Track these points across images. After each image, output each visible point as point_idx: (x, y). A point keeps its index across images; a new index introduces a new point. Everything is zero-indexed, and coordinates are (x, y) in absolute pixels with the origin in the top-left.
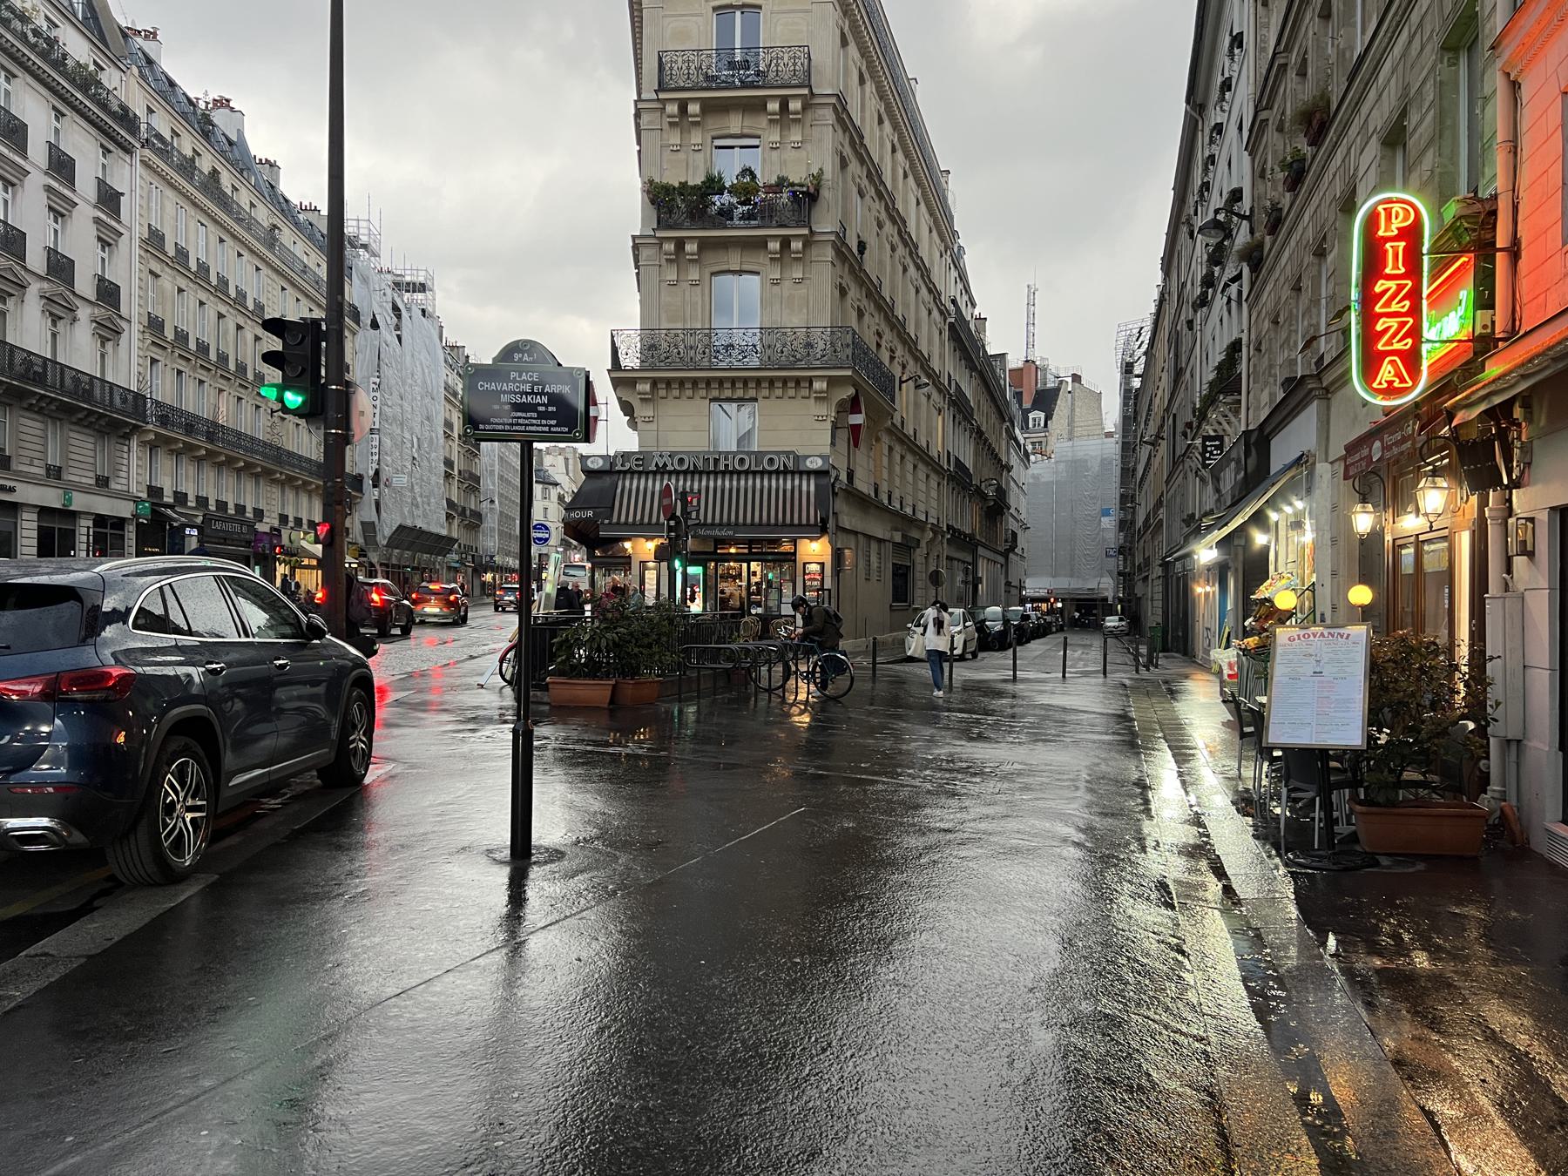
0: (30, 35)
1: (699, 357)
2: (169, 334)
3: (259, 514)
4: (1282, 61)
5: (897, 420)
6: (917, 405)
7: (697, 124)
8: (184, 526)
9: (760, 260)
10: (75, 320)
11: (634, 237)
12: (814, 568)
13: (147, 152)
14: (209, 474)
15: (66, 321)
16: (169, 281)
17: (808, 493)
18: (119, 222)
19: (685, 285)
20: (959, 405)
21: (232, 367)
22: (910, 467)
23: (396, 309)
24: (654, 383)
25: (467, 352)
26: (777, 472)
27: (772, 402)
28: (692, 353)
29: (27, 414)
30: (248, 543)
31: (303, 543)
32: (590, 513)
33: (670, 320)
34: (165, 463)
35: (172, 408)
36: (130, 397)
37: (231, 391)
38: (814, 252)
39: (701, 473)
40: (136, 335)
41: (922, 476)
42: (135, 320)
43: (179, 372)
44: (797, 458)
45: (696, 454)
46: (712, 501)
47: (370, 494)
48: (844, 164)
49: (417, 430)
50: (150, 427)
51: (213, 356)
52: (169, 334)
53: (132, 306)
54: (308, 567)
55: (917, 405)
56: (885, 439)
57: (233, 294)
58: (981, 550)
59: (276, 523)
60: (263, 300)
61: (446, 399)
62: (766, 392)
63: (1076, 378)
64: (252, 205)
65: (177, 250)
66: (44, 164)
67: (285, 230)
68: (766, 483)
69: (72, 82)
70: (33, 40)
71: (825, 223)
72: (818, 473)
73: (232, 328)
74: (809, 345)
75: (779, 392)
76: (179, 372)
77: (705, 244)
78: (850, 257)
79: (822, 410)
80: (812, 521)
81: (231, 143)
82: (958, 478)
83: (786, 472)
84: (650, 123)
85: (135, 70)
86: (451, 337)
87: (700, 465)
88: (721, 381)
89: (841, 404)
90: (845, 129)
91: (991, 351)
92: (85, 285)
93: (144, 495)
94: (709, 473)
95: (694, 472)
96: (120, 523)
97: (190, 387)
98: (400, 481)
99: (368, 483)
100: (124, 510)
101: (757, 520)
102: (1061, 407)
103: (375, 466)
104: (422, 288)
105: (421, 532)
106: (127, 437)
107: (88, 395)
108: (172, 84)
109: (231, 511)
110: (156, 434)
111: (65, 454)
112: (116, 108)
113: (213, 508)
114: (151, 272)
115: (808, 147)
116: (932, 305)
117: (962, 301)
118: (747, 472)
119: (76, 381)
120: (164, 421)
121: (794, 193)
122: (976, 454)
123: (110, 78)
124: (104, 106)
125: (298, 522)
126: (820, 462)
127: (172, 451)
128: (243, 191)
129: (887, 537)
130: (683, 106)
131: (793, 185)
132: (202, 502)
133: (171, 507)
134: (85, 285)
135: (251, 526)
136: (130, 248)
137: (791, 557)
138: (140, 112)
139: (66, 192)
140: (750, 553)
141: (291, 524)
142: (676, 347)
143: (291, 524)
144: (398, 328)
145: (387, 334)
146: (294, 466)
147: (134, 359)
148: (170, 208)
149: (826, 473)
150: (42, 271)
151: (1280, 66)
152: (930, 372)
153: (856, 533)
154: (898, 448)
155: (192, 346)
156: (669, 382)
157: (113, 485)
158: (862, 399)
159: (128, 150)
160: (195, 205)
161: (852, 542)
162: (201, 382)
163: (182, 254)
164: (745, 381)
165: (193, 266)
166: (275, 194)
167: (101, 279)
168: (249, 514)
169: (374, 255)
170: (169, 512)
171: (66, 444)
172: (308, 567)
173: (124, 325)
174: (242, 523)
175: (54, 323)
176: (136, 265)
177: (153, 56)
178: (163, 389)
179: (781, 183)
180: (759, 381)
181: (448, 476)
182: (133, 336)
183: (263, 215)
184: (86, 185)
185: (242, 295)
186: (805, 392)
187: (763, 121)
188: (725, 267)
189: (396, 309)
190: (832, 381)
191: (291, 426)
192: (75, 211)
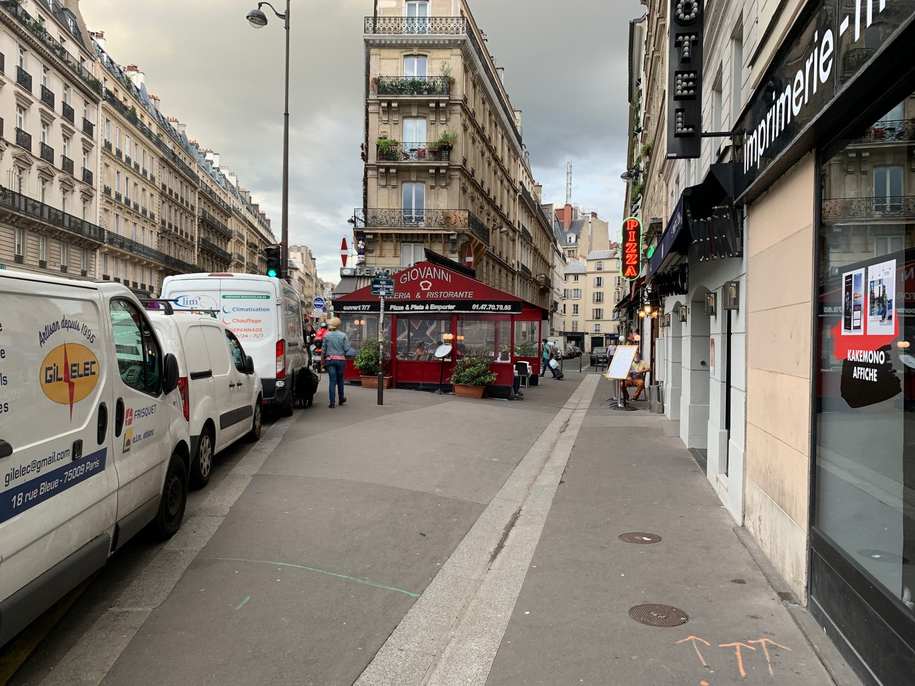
6: (501, 239)
13: (105, 102)
15: (70, 192)
16: (114, 168)
18: (53, 111)
22: (497, 271)
29: (4, 225)
40: (99, 197)
41: (503, 275)
42: (99, 189)
48: (465, 129)
53: (98, 183)
55: (501, 239)
63: (594, 215)
64: (150, 124)
66: (61, 113)
67: (165, 136)
76: (117, 215)
92: (78, 174)
102: (586, 231)
106: (95, 250)
109: (139, 288)
119: (76, 223)
122: (534, 261)
123: (88, 65)
134: (78, 174)
139: (70, 126)
146: (140, 252)
147: (99, 210)
150: (81, 179)
157: (89, 275)
159: (96, 102)
162: (127, 220)
167: (85, 170)
176: (99, 161)
182: (98, 198)
184: (79, 123)
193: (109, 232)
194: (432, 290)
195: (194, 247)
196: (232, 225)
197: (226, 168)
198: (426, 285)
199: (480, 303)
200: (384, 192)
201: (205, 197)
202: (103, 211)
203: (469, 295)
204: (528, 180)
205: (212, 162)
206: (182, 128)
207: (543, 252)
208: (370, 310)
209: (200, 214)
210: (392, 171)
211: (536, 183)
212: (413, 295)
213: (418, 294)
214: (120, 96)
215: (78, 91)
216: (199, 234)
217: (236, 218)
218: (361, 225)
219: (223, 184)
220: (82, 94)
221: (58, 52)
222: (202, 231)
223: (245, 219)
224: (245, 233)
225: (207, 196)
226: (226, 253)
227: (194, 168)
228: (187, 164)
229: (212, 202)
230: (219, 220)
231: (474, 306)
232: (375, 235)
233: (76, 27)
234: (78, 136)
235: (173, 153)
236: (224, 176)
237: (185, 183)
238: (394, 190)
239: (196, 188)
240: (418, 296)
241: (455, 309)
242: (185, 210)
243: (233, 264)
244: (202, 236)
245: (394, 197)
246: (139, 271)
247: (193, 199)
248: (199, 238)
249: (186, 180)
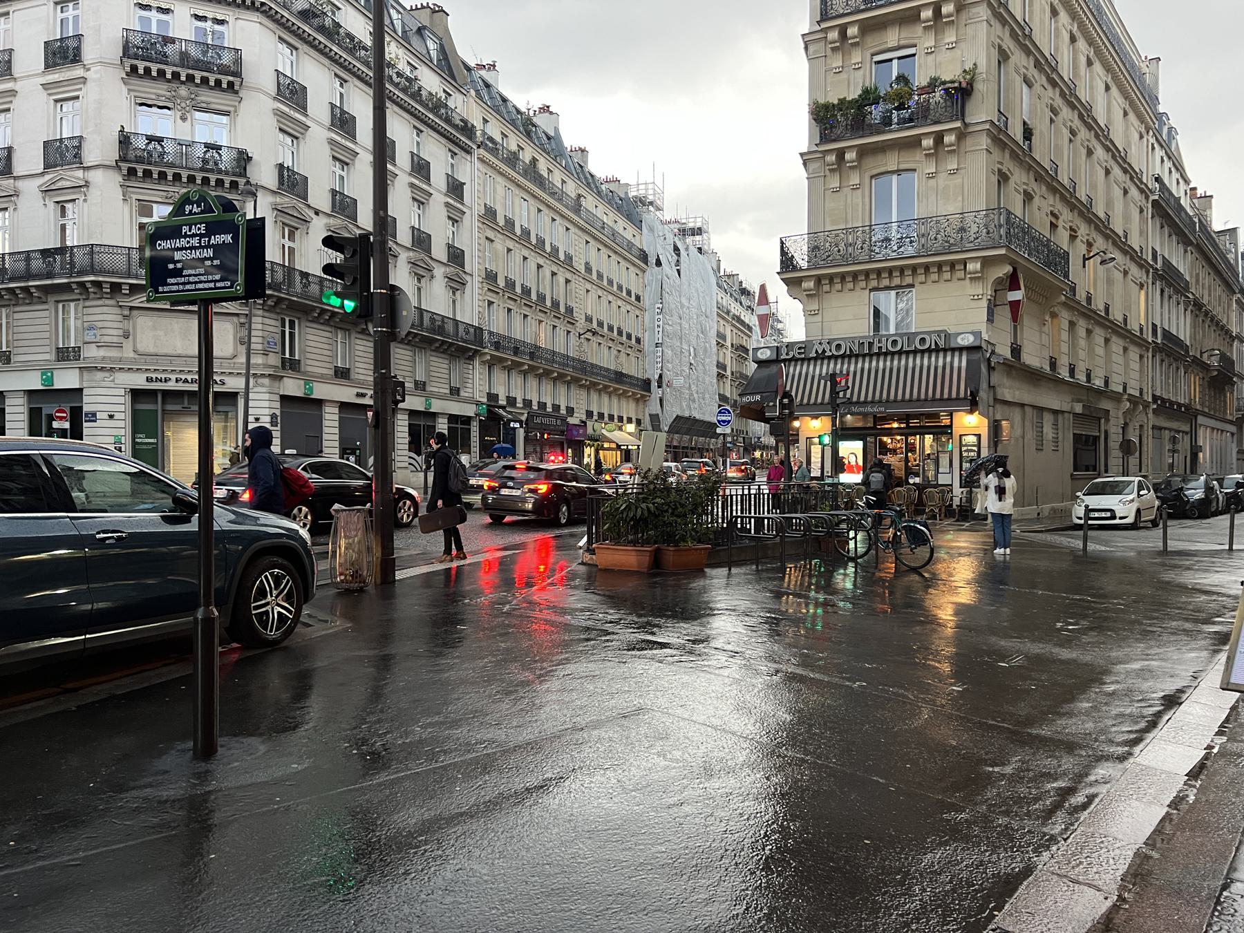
0: (395, 76)
2: (501, 282)
3: (570, 411)
5: (1081, 296)
7: (856, 44)
8: (510, 421)
9: (914, 159)
10: (432, 277)
11: (802, 155)
12: (972, 439)
13: (481, 151)
14: (532, 383)
16: (501, 244)
17: (960, 368)
19: (846, 190)
20: (1168, 279)
21: (548, 303)
22: (1082, 332)
23: (676, 249)
24: (819, 280)
25: (741, 278)
26: (929, 350)
27: (929, 287)
28: (850, 249)
30: (562, 433)
31: (604, 432)
32: (758, 397)
33: (833, 223)
34: (500, 376)
35: (505, 337)
36: (472, 330)
37: (548, 321)
38: (969, 142)
39: (857, 356)
40: (477, 285)
42: (476, 274)
43: (509, 310)
44: (948, 336)
45: (852, 340)
46: (863, 379)
47: (656, 392)
48: (1003, 56)
49: (694, 342)
51: (534, 297)
52: (501, 282)
53: (473, 264)
54: (609, 449)
55: (1110, 281)
56: (1065, 316)
57: (548, 249)
58: (1201, 419)
59: (584, 417)
60: (572, 252)
61: (719, 315)
62: (922, 278)
65: (506, 221)
66: (408, 167)
67: (590, 198)
68: (881, 364)
69: (426, 106)
70: (396, 80)
71: (981, 112)
72: (970, 349)
73: (548, 274)
74: (962, 230)
75: (935, 277)
76: (509, 310)
77: (863, 152)
78: (1013, 146)
79: (978, 289)
80: (962, 395)
81: (549, 138)
82: (1169, 349)
83: (937, 350)
84: (815, 52)
85: (473, 92)
86: (726, 267)
87: (856, 349)
88: (878, 272)
89: (999, 281)
90: (1004, 22)
91: (1217, 225)
92: (439, 252)
93: (485, 400)
94: (864, 356)
95: (850, 356)
96: (467, 420)
97: (517, 321)
98: (679, 382)
99: (654, 384)
100: (470, 410)
101: (907, 396)
103: (659, 371)
104: (698, 231)
105: (695, 420)
107: (441, 330)
108: (505, 100)
109: (549, 409)
111: (428, 372)
112: (458, 122)
113: (535, 407)
115: (962, 45)
116: (1129, 184)
117: (1171, 181)
118: (900, 353)
120: (497, 346)
121: (946, 90)
122: (1194, 326)
124: (448, 120)
125: (601, 416)
126: (971, 338)
128: (556, 172)
129: (1066, 407)
130: (843, 30)
131: (944, 83)
132: (528, 404)
133: (503, 408)
134: (439, 252)
135: (564, 420)
136: (471, 221)
137: (947, 431)
138: (478, 124)
139: (425, 186)
140: (908, 427)
141: (595, 417)
143: (595, 417)
144: (678, 263)
145: (668, 269)
148: (500, 191)
149: (979, 348)
150: (408, 244)
152: (1127, 251)
153: (1022, 405)
154: (1082, 324)
155: (518, 290)
156: (831, 278)
157: (462, 393)
158: (1021, 276)
159: (468, 151)
160: (519, 186)
161: (1016, 414)
163: (510, 223)
164: (902, 270)
165: (518, 231)
166: (583, 171)
168: (563, 411)
169: (658, 209)
170: (501, 411)
171: (428, 365)
172: (609, 449)
173: (468, 278)
174: (557, 418)
175: (419, 281)
177: (491, 81)
178: (497, 323)
179: (933, 84)
180: (914, 269)
181: (720, 376)
183: (571, 189)
185: (555, 250)
186: (961, 274)
187: (919, 29)
188: (883, 169)
189: (676, 249)
190: (987, 262)
191: (595, 345)
192: (431, 200)
193: (491, 333)
204: (1175, 175)
207: (1217, 311)
210: (848, 156)
211: (1200, 192)
220: (443, 141)
224: (728, 331)
233: (442, 49)
234: (439, 200)
246: (605, 398)
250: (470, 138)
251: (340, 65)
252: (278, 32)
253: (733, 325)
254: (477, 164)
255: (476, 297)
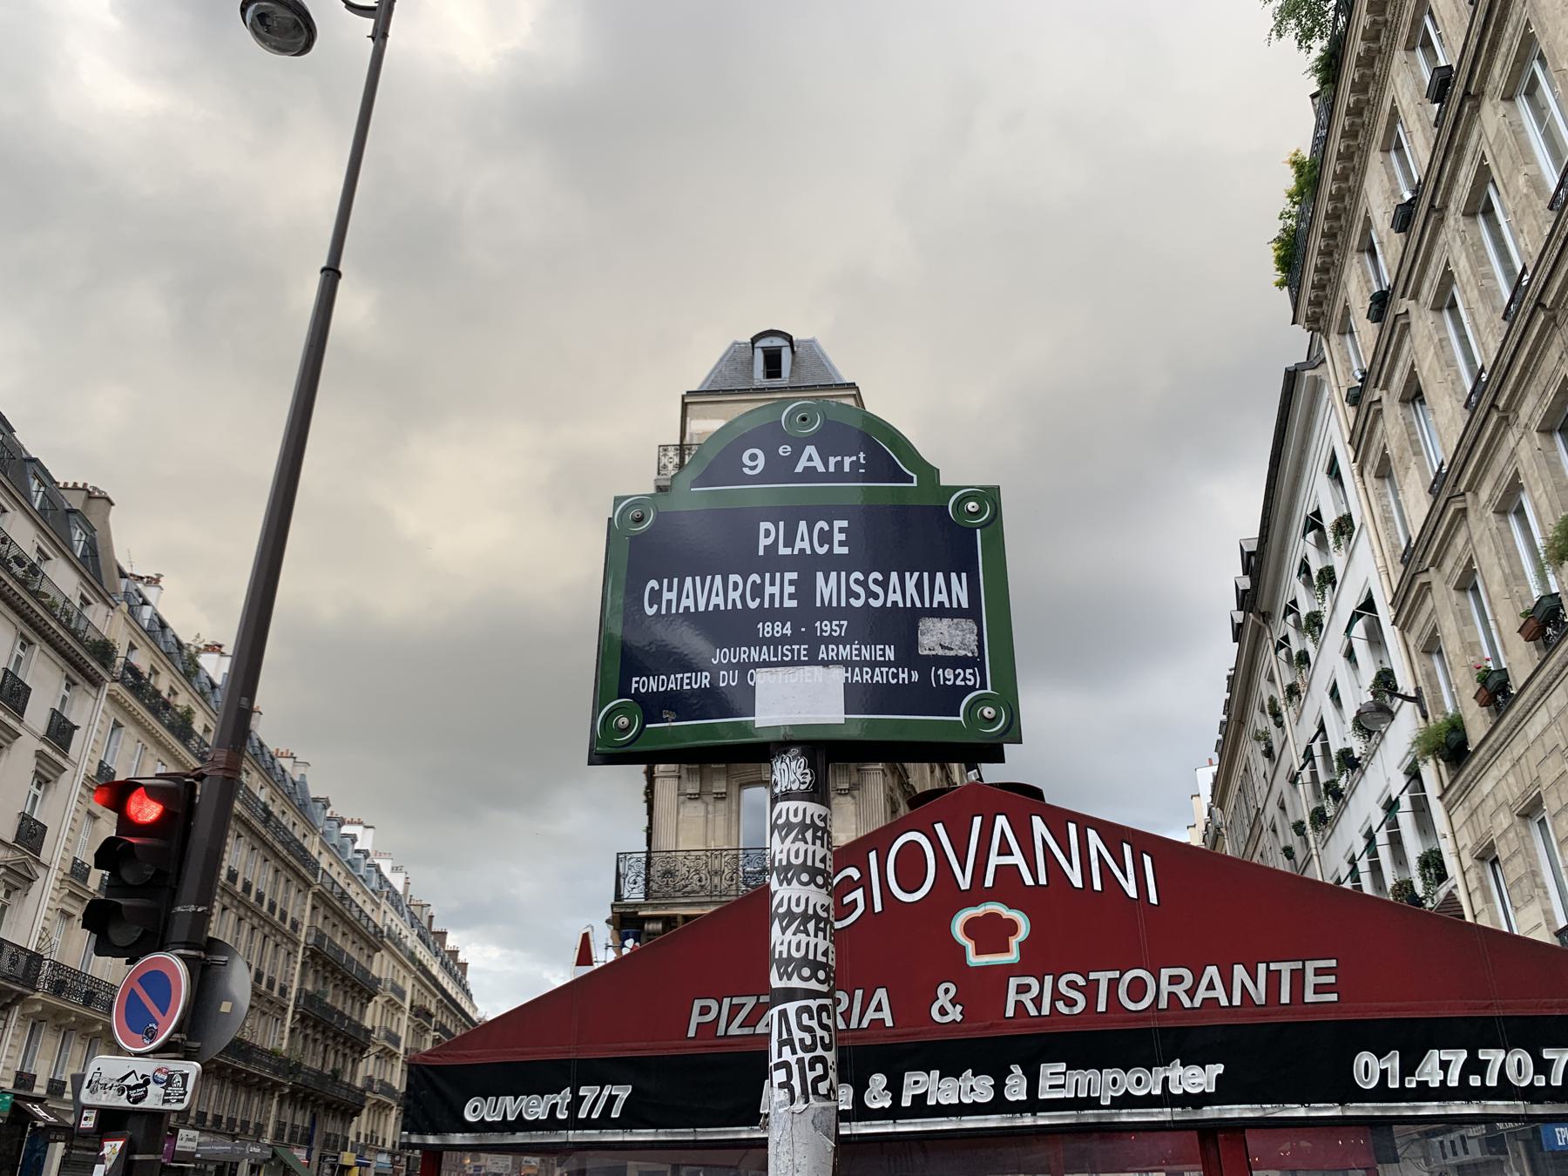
1: (725, 884)
4: (1460, 505)
13: (116, 686)
28: (716, 880)
36: (23, 959)
42: (55, 866)
50: (38, 996)
67: (255, 775)
110: (45, 1004)
114: (89, 812)
127: (60, 1027)
133: (39, 1100)
142: (697, 872)
147: (43, 912)
151: (1458, 511)
173: (40, 872)
194: (1036, 961)
195: (284, 1010)
196: (382, 966)
197: (388, 856)
198: (991, 934)
199: (1410, 1042)
200: (695, 811)
201: (328, 904)
202: (55, 916)
203: (1313, 983)
205: (354, 839)
206: (301, 770)
208: (631, 1118)
209: (311, 940)
212: (912, 1002)
213: (945, 993)
214: (163, 683)
215: (53, 654)
216: (302, 982)
217: (394, 955)
218: (633, 894)
219: (375, 883)
220: (61, 661)
221: (19, 571)
222: (311, 974)
223: (412, 956)
225: (332, 905)
226: (359, 1027)
227: (313, 846)
228: (297, 835)
229: (342, 916)
230: (355, 955)
231: (1368, 1067)
232: (669, 921)
235: (265, 809)
236: (377, 868)
237: (285, 873)
238: (721, 805)
239: (309, 885)
240: (946, 1008)
241: (1226, 1091)
242: (276, 929)
243: (372, 1050)
244: (309, 987)
245: (720, 821)
247: (300, 909)
248: (300, 990)
249: (288, 865)
250: (105, 666)
251: (125, 709)
252: (21, 627)
253: (417, 978)
254: (104, 702)
255: (46, 902)
